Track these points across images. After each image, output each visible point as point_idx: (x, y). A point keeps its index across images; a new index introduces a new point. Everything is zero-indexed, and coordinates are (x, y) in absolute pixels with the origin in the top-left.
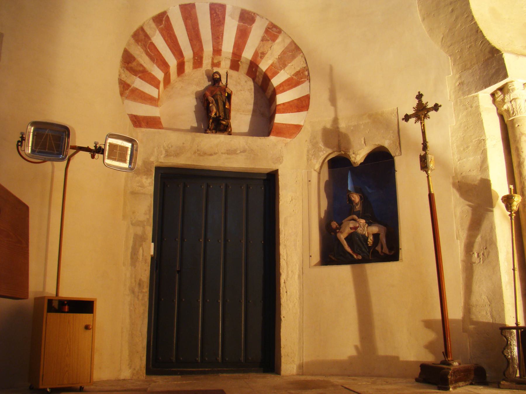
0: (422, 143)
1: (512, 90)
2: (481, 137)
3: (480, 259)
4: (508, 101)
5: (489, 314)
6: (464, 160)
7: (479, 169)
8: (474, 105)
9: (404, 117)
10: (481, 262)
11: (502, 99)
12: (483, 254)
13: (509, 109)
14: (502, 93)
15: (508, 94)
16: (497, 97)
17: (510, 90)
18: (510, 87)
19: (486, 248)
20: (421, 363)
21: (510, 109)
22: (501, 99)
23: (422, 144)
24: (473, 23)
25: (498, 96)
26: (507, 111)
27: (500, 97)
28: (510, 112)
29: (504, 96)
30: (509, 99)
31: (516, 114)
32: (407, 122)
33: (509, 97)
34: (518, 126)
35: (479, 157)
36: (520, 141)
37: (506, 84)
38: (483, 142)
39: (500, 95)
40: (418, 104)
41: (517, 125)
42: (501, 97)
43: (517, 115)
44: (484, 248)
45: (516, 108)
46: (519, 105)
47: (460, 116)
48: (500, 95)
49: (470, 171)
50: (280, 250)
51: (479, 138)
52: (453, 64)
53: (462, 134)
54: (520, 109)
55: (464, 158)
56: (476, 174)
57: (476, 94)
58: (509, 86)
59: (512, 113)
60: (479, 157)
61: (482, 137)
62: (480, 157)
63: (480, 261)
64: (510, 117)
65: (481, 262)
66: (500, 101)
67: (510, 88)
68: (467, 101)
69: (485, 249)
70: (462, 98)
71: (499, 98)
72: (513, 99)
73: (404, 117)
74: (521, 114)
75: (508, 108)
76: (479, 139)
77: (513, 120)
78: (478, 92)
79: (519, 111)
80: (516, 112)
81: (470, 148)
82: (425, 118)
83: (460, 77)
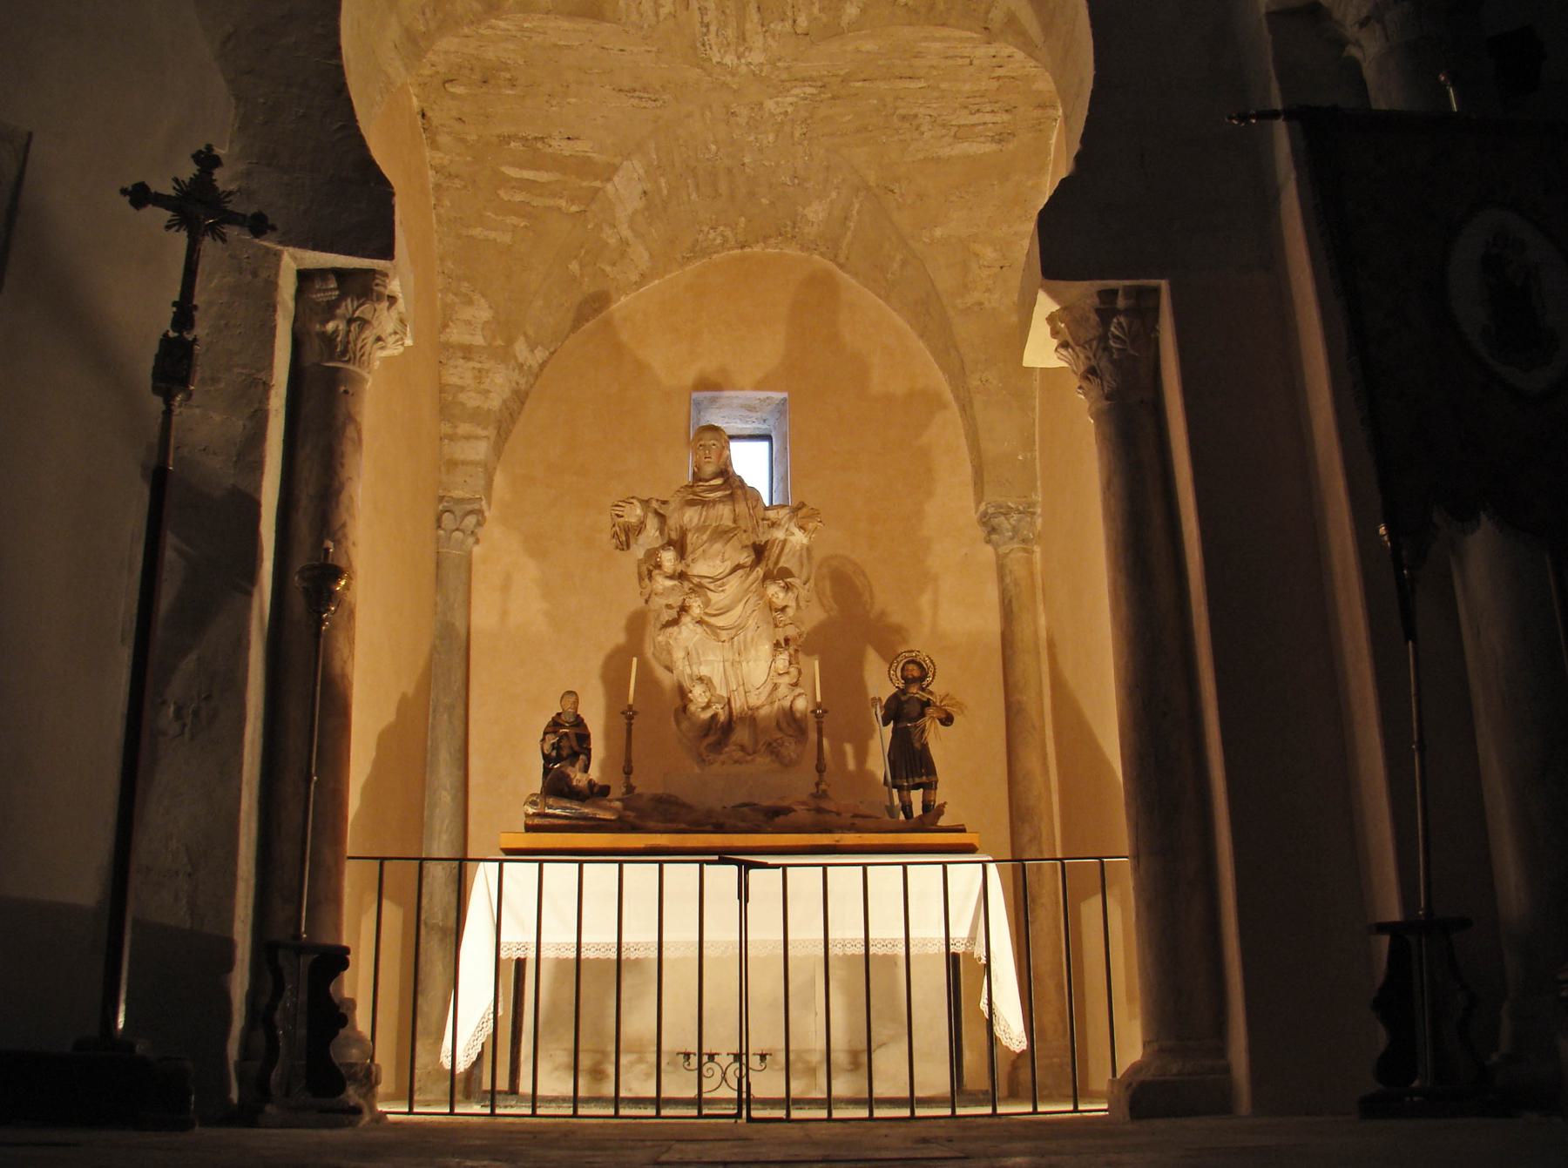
0: (177, 299)
1: (377, 296)
2: (259, 371)
3: (184, 725)
4: (344, 316)
5: (184, 902)
6: (197, 411)
7: (234, 459)
8: (264, 274)
9: (130, 189)
10: (187, 736)
11: (328, 301)
12: (196, 713)
13: (338, 336)
14: (338, 288)
15: (358, 299)
16: (317, 287)
17: (375, 294)
18: (377, 285)
19: (208, 698)
20: (349, 1018)
21: (339, 339)
22: (325, 300)
23: (175, 304)
24: (333, 62)
25: (324, 287)
26: (329, 340)
27: (326, 294)
28: (336, 347)
29: (342, 298)
30: (351, 312)
31: (350, 360)
32: (1047, 319)
33: (355, 306)
34: (346, 392)
35: (239, 425)
36: (343, 434)
37: (371, 273)
38: (261, 387)
39: (331, 290)
40: (195, 180)
41: (342, 389)
42: (331, 296)
43: (352, 362)
44: (203, 696)
45: (355, 345)
46: (363, 340)
47: (216, 281)
48: (331, 290)
49: (204, 450)
50: (280, 468)
51: (253, 371)
52: (236, 126)
53: (208, 335)
54: (363, 351)
55: (198, 407)
56: (221, 468)
57: (279, 247)
58: (377, 281)
59: (341, 351)
60: (241, 423)
61: (262, 373)
62: (244, 425)
63: (182, 733)
64: (331, 358)
65: (187, 736)
66: (318, 304)
67: (376, 288)
68: (246, 252)
69: (205, 698)
70: (236, 233)
71: (322, 295)
72: (359, 318)
73: (130, 189)
74: (360, 367)
75: (336, 331)
76: (253, 374)
77: (338, 369)
78: (288, 246)
79: (358, 355)
80: (352, 356)
81: (222, 385)
82: (209, 233)
83: (248, 174)
